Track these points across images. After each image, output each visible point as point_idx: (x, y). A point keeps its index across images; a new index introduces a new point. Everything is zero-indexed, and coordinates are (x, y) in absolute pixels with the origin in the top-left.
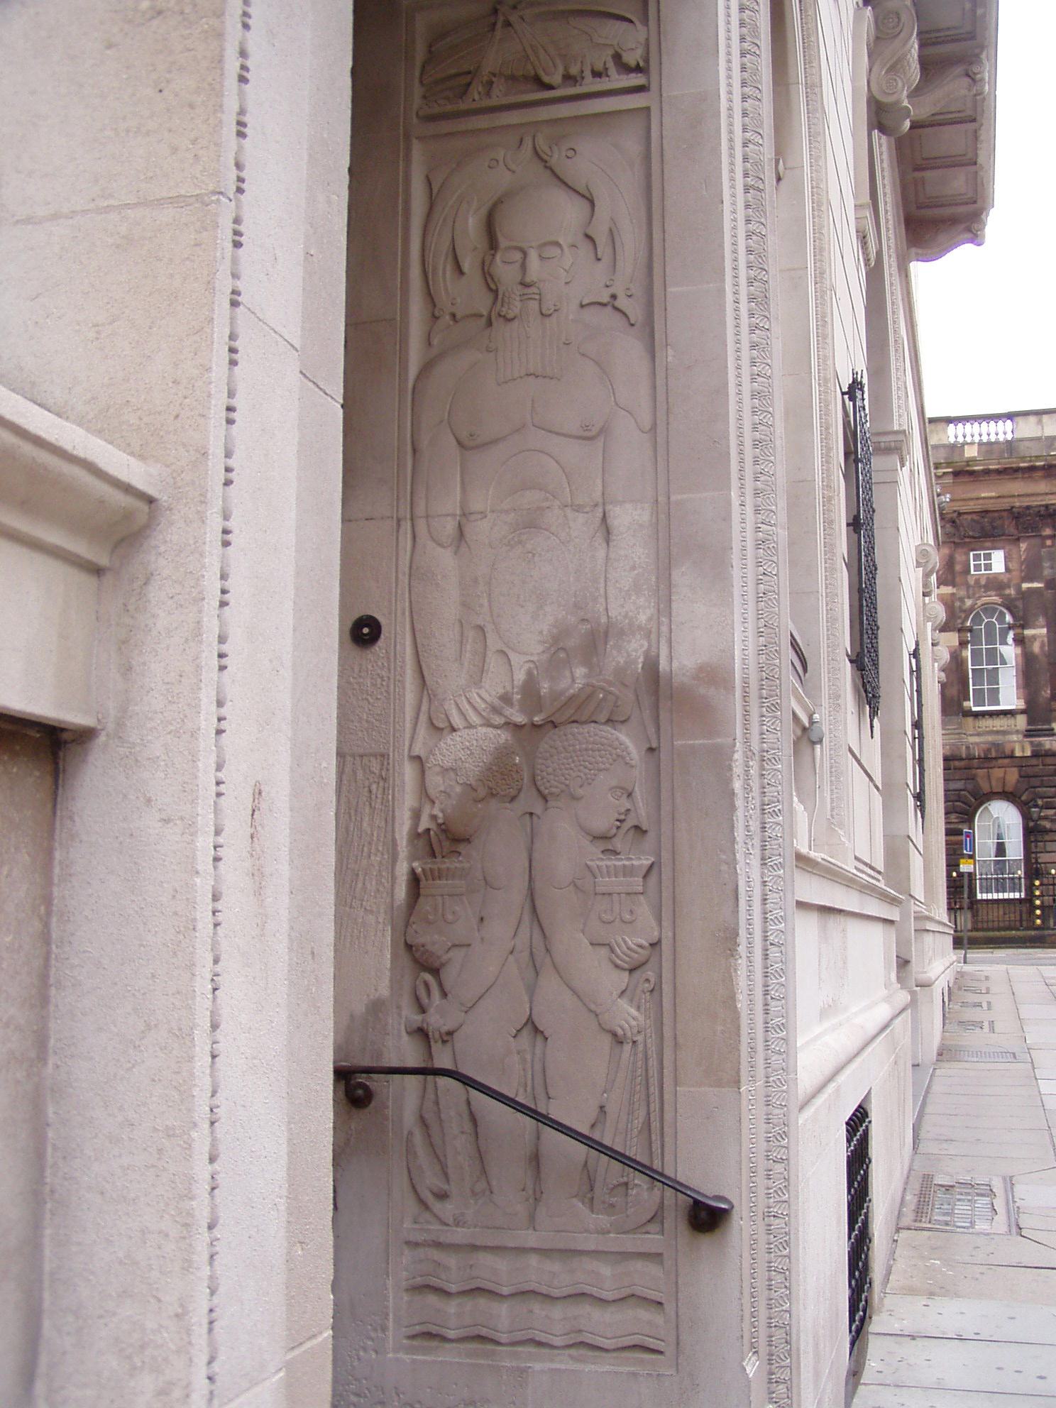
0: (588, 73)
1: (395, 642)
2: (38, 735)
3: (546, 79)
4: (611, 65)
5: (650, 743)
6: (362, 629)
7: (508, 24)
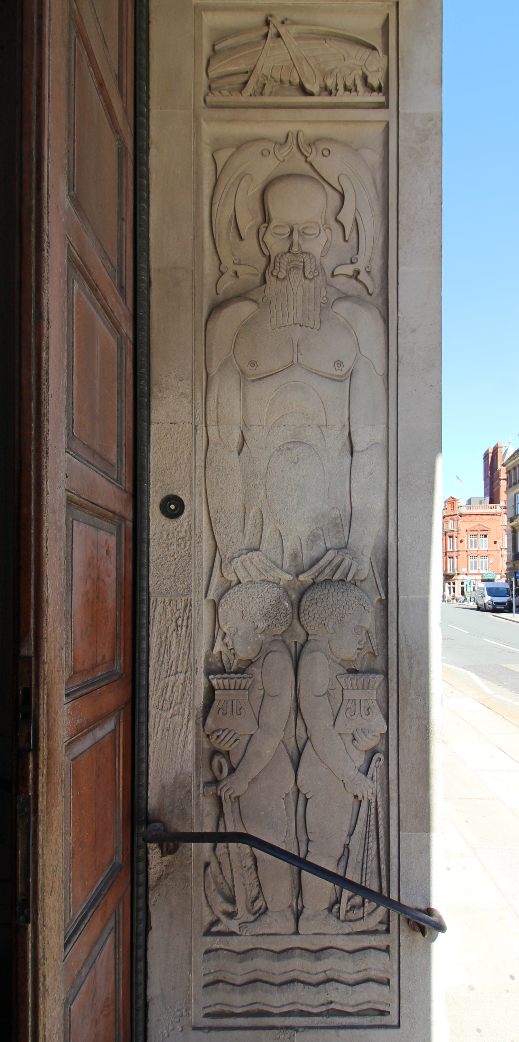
0: (341, 88)
1: (195, 515)
2: (142, 265)
3: (308, 87)
4: (359, 83)
5: (381, 596)
6: (171, 509)
7: (279, 35)
